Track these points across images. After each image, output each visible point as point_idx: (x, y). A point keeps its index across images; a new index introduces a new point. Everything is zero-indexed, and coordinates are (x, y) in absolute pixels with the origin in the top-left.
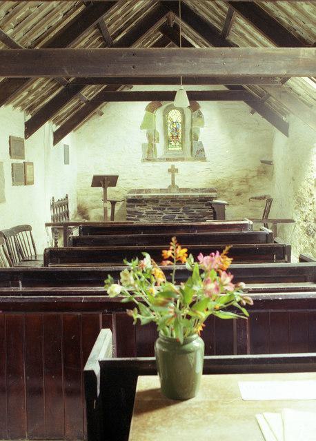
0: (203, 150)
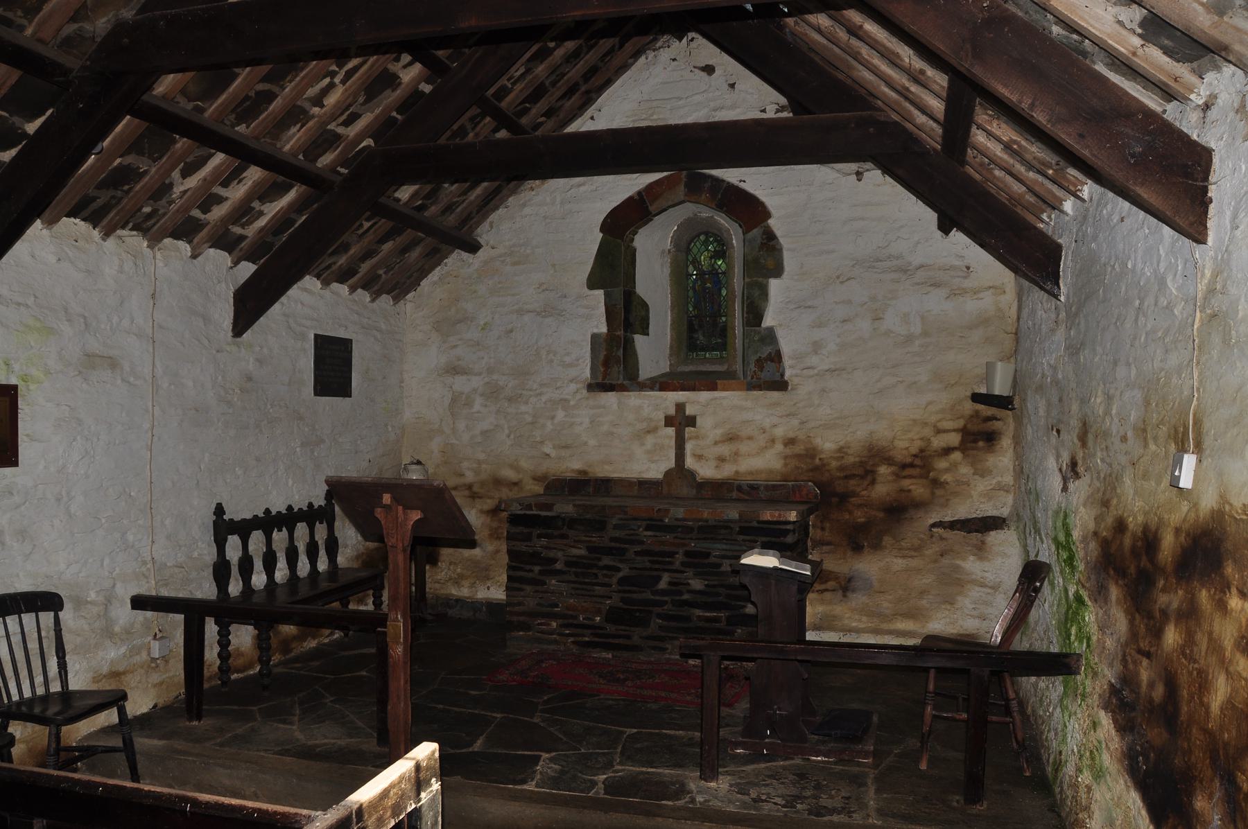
0: (777, 357)
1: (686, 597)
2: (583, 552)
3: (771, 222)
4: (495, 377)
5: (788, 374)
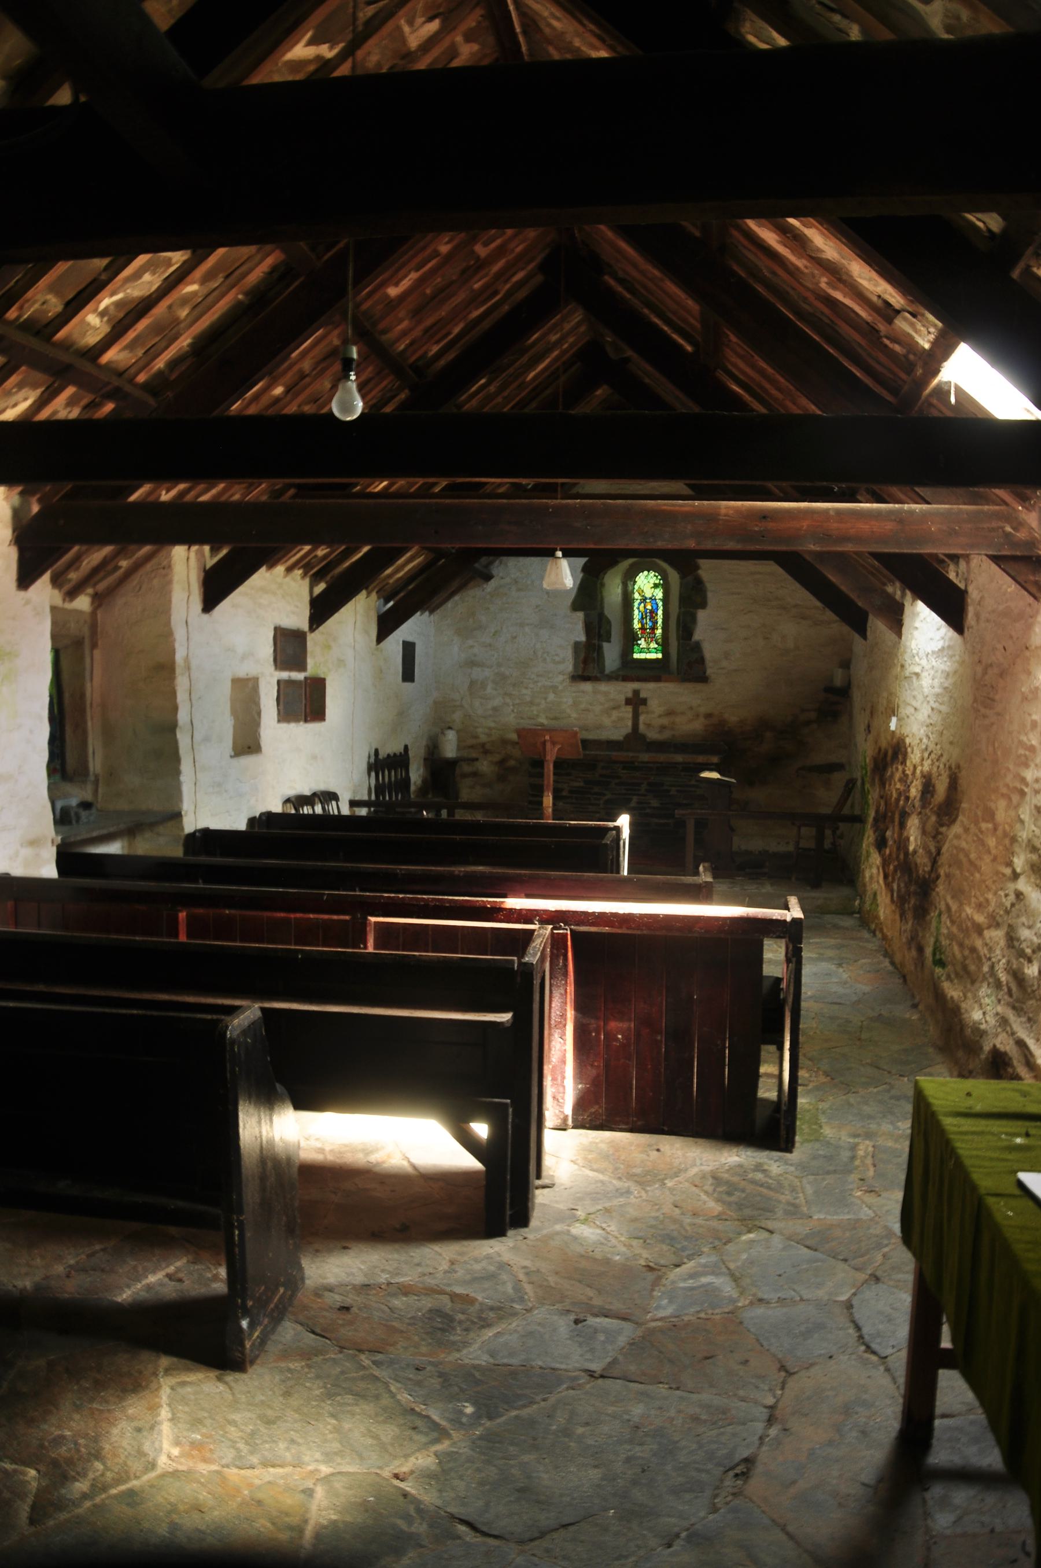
0: (701, 660)
1: (648, 811)
2: (582, 784)
3: (700, 572)
4: (502, 669)
5: (709, 672)
